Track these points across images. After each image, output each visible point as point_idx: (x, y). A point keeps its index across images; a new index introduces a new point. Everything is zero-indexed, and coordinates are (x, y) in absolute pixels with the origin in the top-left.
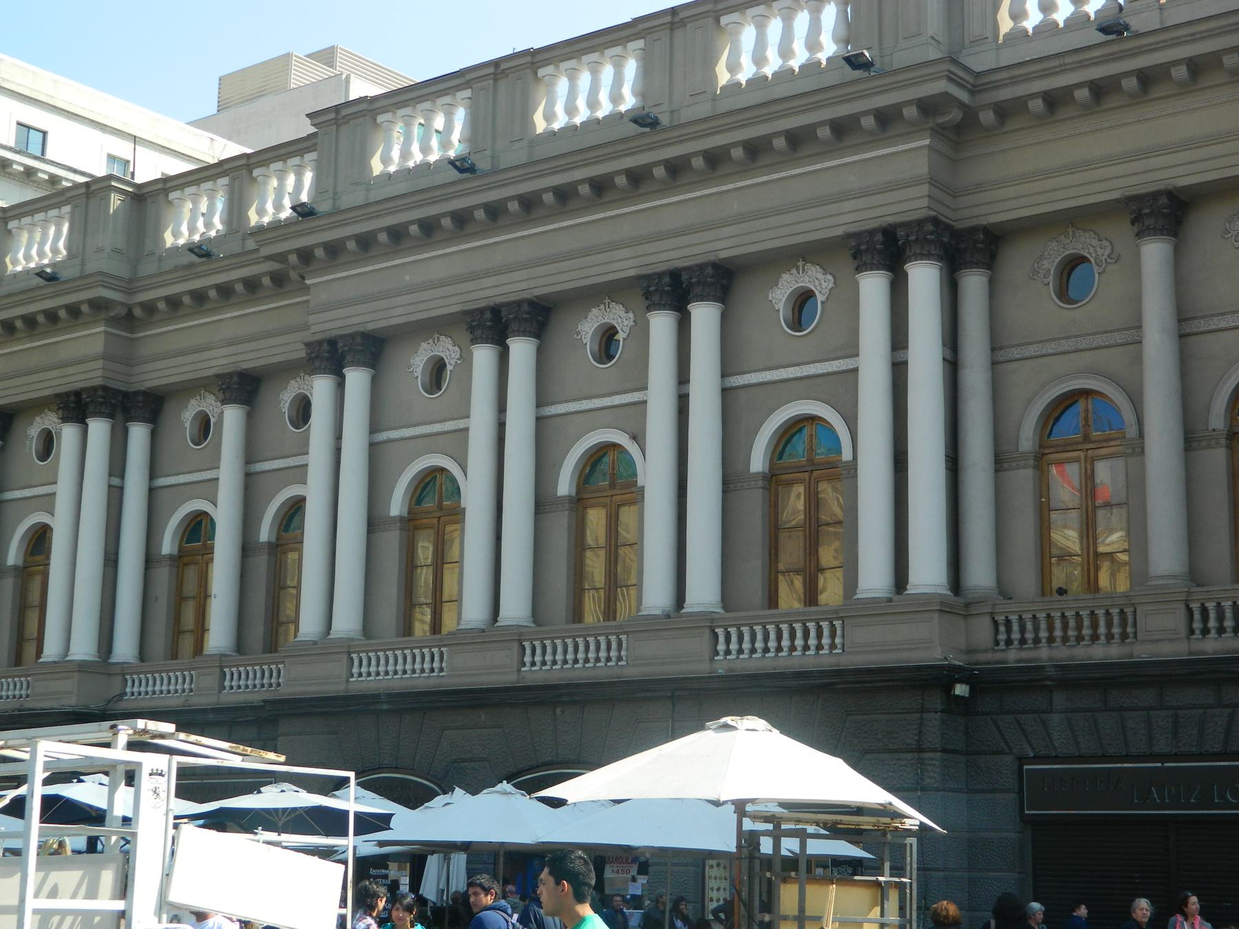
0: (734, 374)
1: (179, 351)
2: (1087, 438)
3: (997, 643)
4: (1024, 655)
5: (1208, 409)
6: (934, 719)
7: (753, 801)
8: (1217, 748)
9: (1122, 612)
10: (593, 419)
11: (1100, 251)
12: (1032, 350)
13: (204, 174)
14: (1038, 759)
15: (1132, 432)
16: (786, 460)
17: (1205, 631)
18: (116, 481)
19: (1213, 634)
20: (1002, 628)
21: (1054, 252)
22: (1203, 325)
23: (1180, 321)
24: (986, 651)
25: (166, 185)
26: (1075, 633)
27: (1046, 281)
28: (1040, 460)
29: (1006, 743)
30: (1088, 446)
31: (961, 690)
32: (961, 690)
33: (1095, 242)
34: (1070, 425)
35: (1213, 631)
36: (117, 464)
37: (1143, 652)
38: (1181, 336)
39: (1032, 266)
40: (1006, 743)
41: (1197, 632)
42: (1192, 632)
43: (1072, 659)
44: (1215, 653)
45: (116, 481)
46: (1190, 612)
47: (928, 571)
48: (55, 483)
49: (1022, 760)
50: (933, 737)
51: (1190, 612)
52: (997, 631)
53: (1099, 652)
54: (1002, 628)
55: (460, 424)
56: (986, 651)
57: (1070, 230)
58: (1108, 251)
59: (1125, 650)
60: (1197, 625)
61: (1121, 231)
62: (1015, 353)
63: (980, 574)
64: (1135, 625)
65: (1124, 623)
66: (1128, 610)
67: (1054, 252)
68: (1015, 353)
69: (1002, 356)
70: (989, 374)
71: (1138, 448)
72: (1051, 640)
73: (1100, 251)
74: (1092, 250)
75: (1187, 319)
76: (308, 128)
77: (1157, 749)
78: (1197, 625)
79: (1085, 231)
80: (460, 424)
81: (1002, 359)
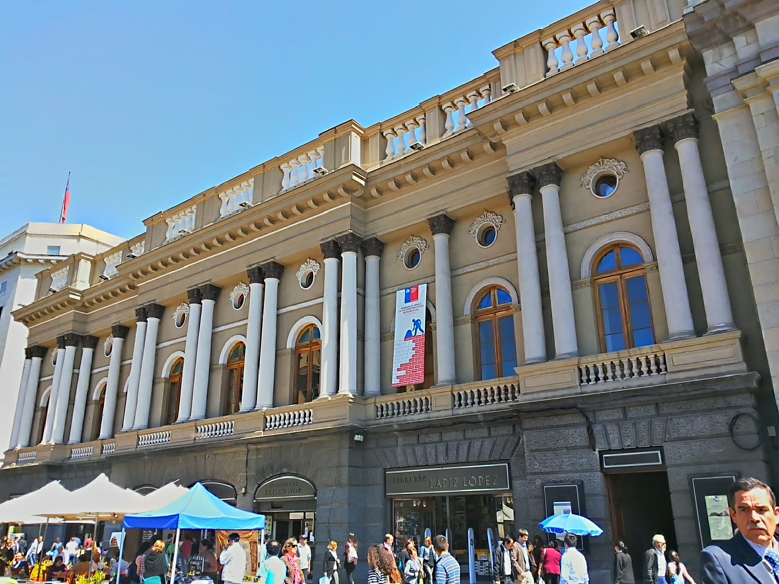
0: (217, 327)
1: (395, 216)
3: (582, 381)
4: (388, 420)
6: (345, 453)
7: (127, 513)
8: (464, 460)
9: (426, 399)
10: (301, 313)
11: (422, 245)
12: (502, 259)
13: (114, 250)
14: (392, 469)
18: (76, 371)
19: (602, 381)
20: (617, 368)
22: (461, 271)
23: (451, 271)
24: (372, 420)
25: (103, 255)
26: (408, 410)
27: (587, 187)
29: (379, 462)
31: (358, 438)
32: (358, 438)
33: (616, 163)
36: (77, 365)
37: (433, 415)
38: (452, 277)
39: (396, 256)
40: (379, 462)
42: (582, 381)
45: (76, 371)
47: (347, 387)
48: (248, 318)
49: (385, 470)
50: (345, 461)
51: (580, 370)
52: (581, 375)
53: (417, 417)
54: (617, 368)
55: (319, 300)
56: (372, 420)
58: (425, 245)
59: (427, 415)
60: (584, 378)
62: (390, 290)
64: (665, 363)
65: (657, 363)
68: (390, 290)
70: (379, 299)
72: (606, 378)
73: (422, 245)
75: (454, 270)
76: (144, 229)
77: (440, 462)
78: (584, 378)
81: (458, 274)
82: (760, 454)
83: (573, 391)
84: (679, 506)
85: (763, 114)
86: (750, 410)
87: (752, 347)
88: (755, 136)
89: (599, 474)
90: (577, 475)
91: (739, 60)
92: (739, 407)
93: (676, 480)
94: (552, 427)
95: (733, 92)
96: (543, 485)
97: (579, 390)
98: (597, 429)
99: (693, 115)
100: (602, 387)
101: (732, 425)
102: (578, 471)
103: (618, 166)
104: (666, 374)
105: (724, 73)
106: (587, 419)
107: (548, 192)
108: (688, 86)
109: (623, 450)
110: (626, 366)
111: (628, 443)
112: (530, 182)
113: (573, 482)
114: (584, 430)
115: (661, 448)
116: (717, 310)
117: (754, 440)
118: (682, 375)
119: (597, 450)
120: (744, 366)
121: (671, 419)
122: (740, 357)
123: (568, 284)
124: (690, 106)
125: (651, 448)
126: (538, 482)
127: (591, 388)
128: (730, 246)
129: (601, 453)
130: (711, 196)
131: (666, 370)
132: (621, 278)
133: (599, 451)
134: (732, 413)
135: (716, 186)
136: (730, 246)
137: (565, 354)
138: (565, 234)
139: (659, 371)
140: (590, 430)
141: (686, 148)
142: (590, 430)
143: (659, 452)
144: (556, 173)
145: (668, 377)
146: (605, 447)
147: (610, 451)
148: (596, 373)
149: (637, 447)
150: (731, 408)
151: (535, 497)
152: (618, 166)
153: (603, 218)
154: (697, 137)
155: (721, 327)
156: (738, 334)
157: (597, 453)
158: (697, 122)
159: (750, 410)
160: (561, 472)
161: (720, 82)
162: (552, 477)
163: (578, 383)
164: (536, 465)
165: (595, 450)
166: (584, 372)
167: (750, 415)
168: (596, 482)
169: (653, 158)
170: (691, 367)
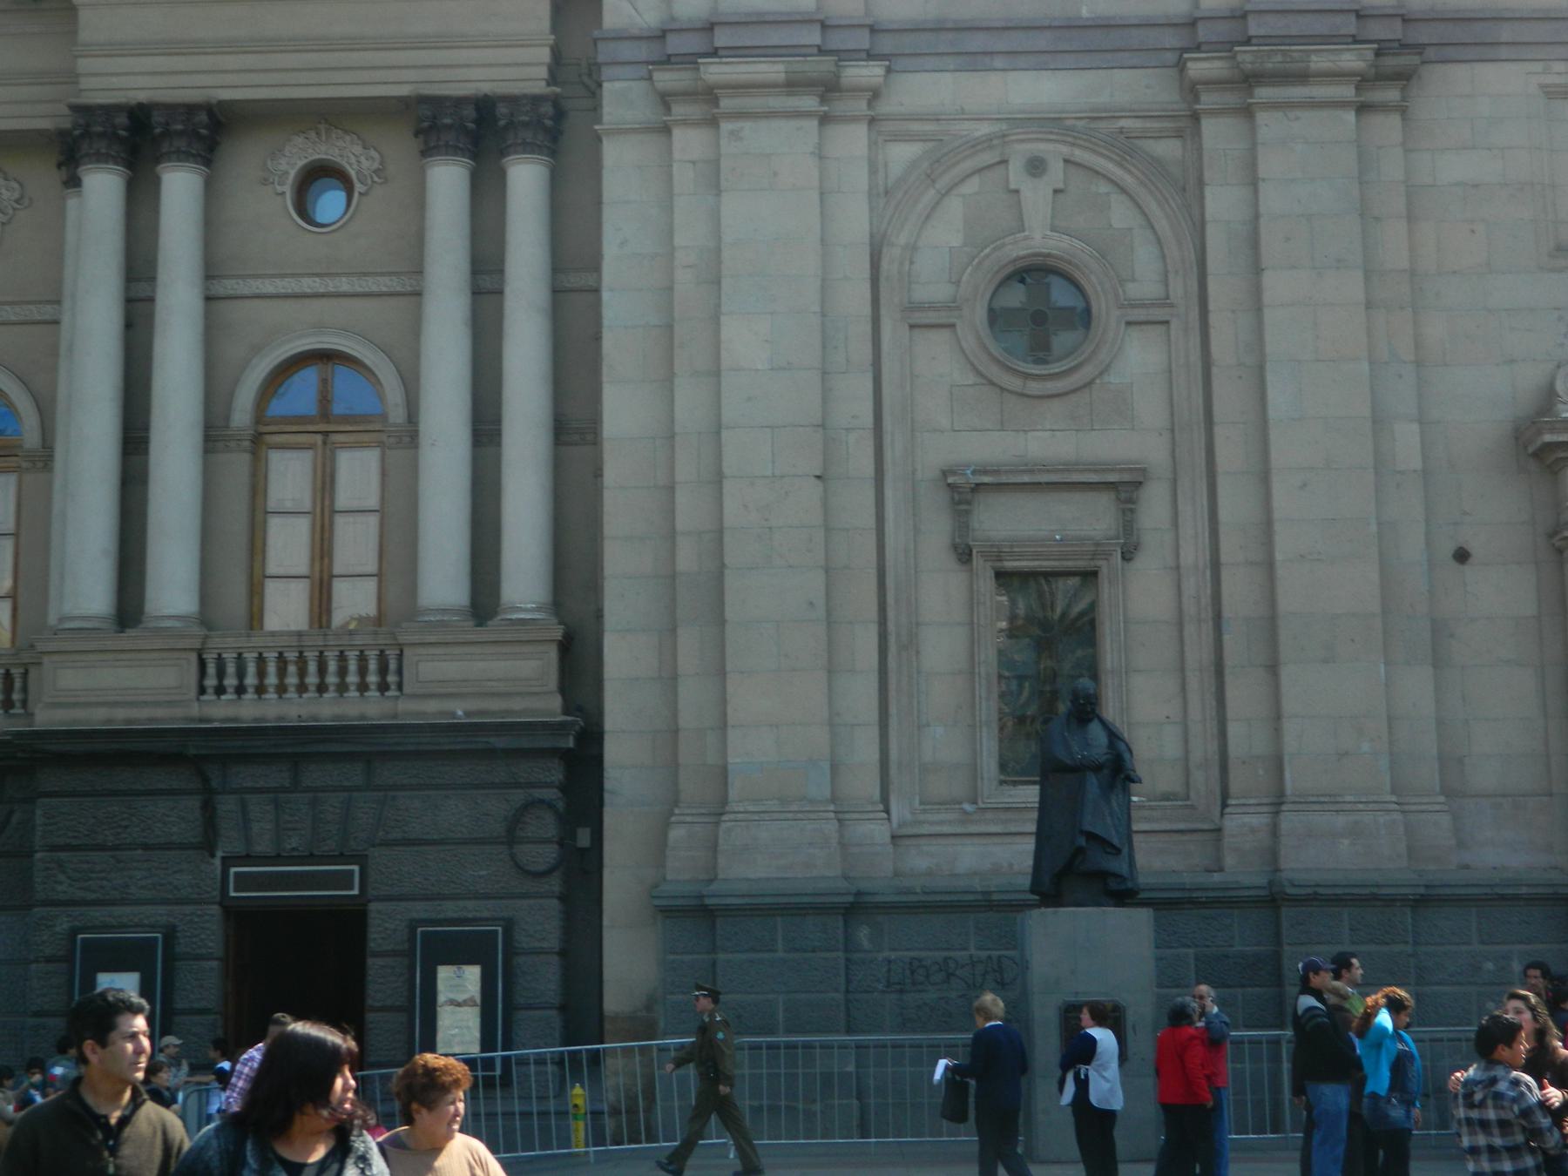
2: (325, 414)
3: (202, 690)
5: (236, 382)
15: (397, 415)
16: (277, 407)
17: (240, 690)
20: (292, 669)
21: (298, 153)
27: (279, 189)
28: (258, 443)
30: (327, 429)
33: (358, 149)
34: (301, 393)
35: (251, 690)
41: (210, 691)
43: (363, 717)
44: (256, 720)
46: (202, 664)
51: (202, 664)
54: (292, 669)
57: (322, 127)
60: (211, 682)
61: (398, 145)
63: (173, 588)
64: (400, 672)
65: (383, 670)
66: (392, 654)
67: (298, 153)
69: (220, 288)
71: (407, 436)
72: (260, 690)
74: (353, 160)
78: (211, 682)
79: (346, 132)
80: (48, 312)
82: (555, 884)
83: (179, 712)
84: (382, 981)
85: (694, 163)
86: (550, 794)
87: (578, 656)
88: (669, 209)
89: (215, 910)
90: (162, 909)
91: (673, 19)
92: (532, 785)
93: (385, 926)
94: (115, 793)
95: (643, 84)
96: (74, 932)
97: (195, 710)
98: (227, 805)
99: (556, 101)
100: (248, 711)
101: (514, 823)
102: (165, 902)
103: (363, 159)
104: (397, 698)
105: (635, 32)
106: (206, 780)
107: (180, 186)
108: (555, 28)
109: (277, 859)
110: (312, 667)
111: (293, 842)
112: (139, 138)
113: (153, 927)
114: (193, 803)
115: (361, 859)
116: (524, 579)
117: (546, 855)
118: (432, 706)
119: (219, 854)
120: (556, 702)
121: (394, 798)
122: (552, 682)
123: (197, 436)
124: (553, 79)
125: (341, 858)
126: (63, 925)
127: (223, 711)
128: (574, 430)
129: (227, 862)
130: (558, 293)
131: (400, 686)
132: (325, 443)
133: (223, 858)
134: (518, 796)
135: (574, 280)
136: (574, 430)
137: (170, 617)
138: (208, 299)
139: (383, 687)
140: (208, 808)
141: (525, 178)
142: (208, 808)
143: (356, 868)
144: (208, 131)
145: (404, 706)
146: (240, 849)
147: (248, 859)
148: (241, 674)
149: (312, 855)
150: (517, 785)
151: (49, 960)
152: (363, 159)
153: (308, 285)
154: (553, 153)
155: (526, 610)
156: (558, 633)
157: (217, 862)
158: (560, 114)
159: (550, 794)
160: (123, 902)
161: (627, 51)
162: (98, 914)
163: (193, 693)
164: (61, 883)
165: (213, 856)
166: (211, 669)
167: (551, 806)
168: (207, 932)
169: (448, 181)
170: (450, 690)
